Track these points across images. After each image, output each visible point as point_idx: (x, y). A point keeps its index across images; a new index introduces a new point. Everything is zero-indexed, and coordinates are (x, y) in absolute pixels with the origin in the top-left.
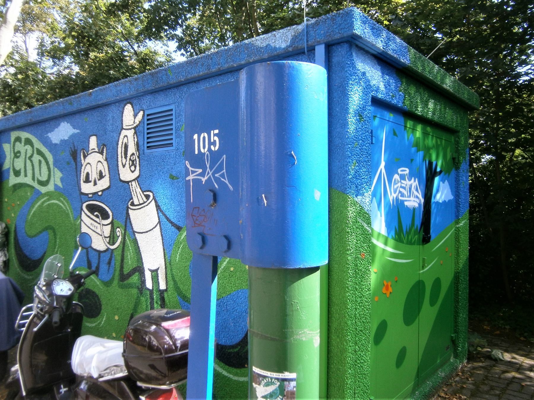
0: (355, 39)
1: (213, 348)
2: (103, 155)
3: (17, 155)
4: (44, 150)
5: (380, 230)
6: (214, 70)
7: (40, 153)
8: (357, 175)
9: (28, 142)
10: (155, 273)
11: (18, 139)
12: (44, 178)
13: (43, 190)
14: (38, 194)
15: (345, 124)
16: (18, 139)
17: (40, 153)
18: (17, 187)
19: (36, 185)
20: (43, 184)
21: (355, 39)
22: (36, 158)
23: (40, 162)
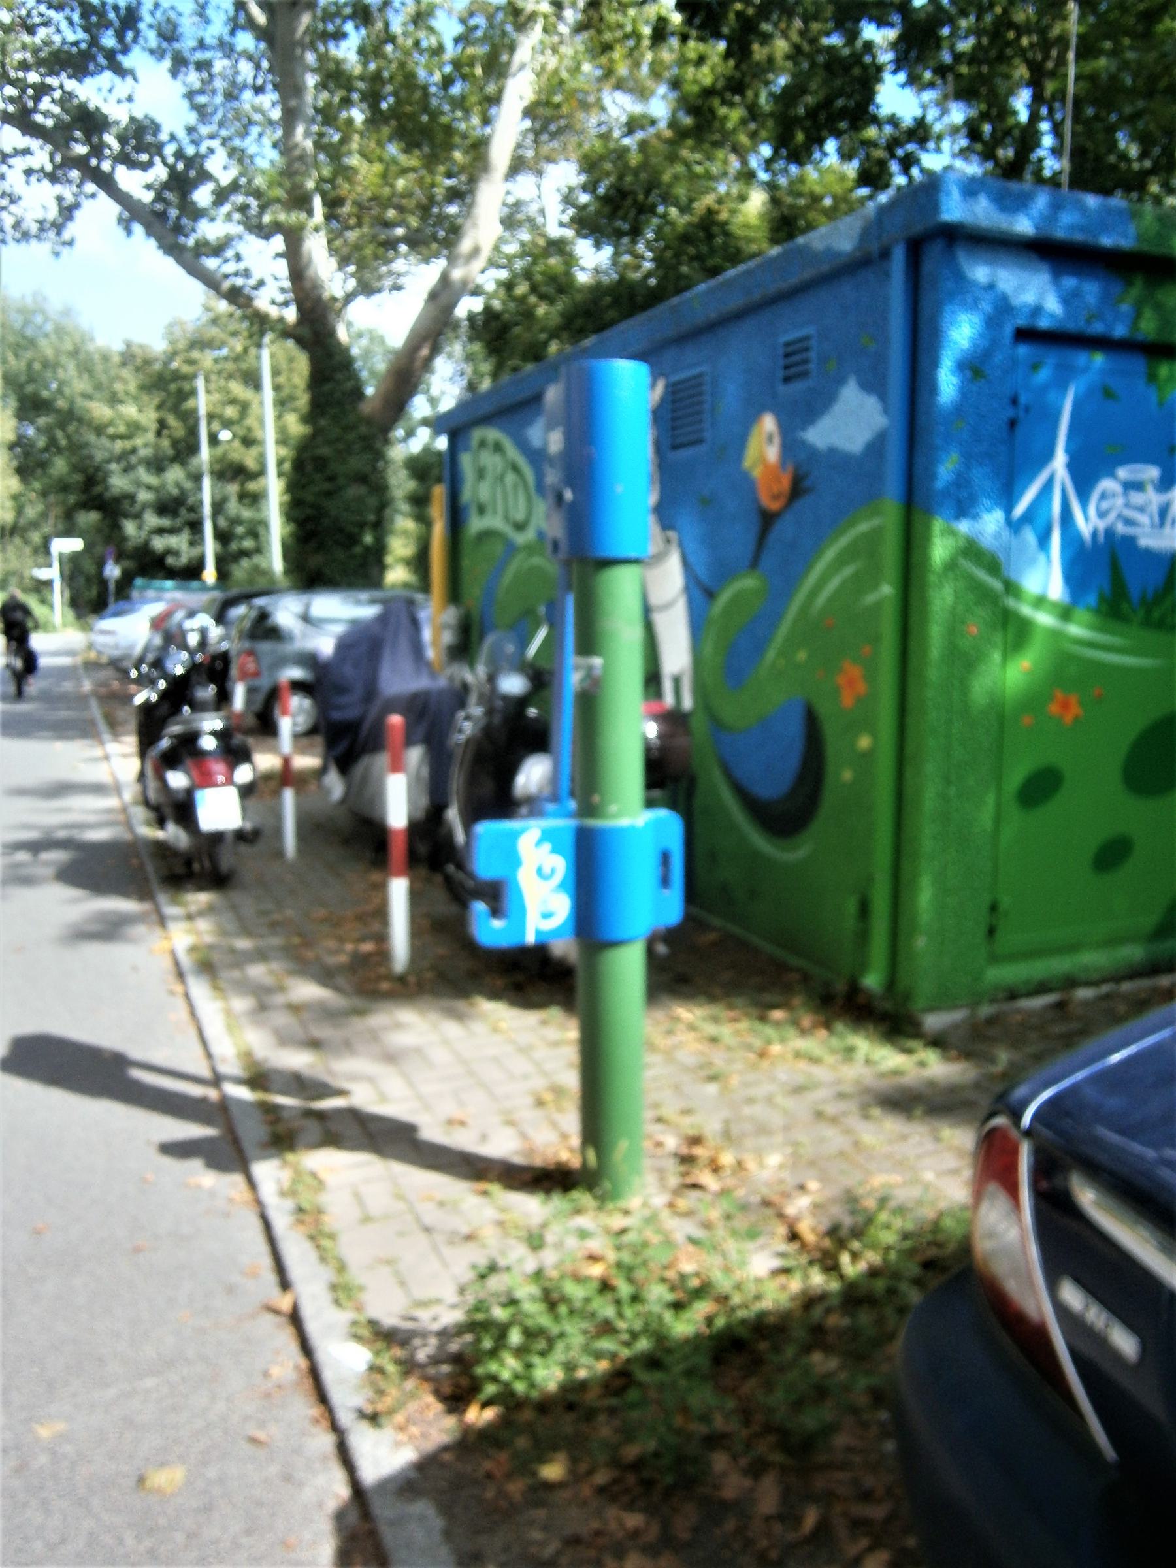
0: (177, 963)
1: (620, 489)
2: (1012, 1190)
3: (481, 474)
4: (522, 462)
5: (1046, 586)
6: (757, 295)
7: (515, 468)
8: (961, 481)
9: (498, 448)
10: (677, 681)
11: (483, 444)
12: (520, 516)
13: (521, 539)
14: (511, 548)
15: (933, 389)
16: (483, 444)
17: (515, 468)
18: (487, 535)
19: (507, 530)
20: (520, 527)
21: (177, 963)
22: (510, 478)
23: (515, 487)
